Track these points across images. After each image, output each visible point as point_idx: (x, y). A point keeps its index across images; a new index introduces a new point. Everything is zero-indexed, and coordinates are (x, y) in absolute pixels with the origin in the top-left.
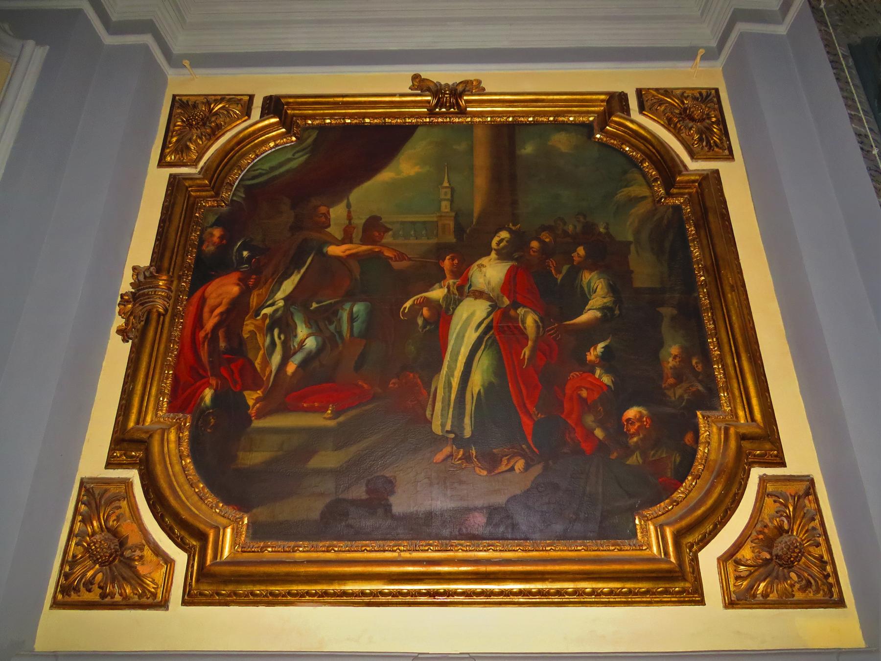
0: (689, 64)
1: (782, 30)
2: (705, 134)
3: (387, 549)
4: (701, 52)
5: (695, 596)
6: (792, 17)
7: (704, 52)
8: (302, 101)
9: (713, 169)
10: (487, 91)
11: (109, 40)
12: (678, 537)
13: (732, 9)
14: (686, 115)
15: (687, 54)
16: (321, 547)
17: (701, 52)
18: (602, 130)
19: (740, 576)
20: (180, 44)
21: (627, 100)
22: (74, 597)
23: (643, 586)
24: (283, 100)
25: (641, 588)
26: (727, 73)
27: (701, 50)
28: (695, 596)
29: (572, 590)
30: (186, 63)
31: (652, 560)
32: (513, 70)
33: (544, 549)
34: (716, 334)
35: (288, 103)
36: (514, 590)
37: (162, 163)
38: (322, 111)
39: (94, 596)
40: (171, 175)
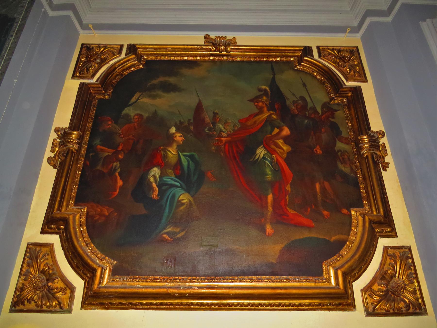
0: (343, 35)
1: (389, 19)
2: (352, 67)
3: (320, 281)
4: (349, 29)
5: (351, 306)
6: (71, 16)
7: (350, 30)
8: (145, 47)
9: (358, 86)
10: (237, 44)
11: (51, 13)
12: (345, 275)
13: (366, 10)
14: (342, 59)
15: (341, 30)
16: (188, 280)
17: (349, 29)
18: (300, 65)
19: (48, 292)
20: (87, 19)
21: (312, 50)
22: (18, 308)
23: (316, 302)
24: (137, 46)
25: (315, 303)
26: (363, 38)
27: (348, 29)
28: (351, 306)
29: (318, 303)
30: (91, 26)
31: (333, 288)
32: (266, 35)
33: (283, 281)
34: (361, 168)
35: (139, 48)
36: (235, 303)
37: (73, 77)
38: (156, 52)
39: (32, 306)
40: (81, 83)
